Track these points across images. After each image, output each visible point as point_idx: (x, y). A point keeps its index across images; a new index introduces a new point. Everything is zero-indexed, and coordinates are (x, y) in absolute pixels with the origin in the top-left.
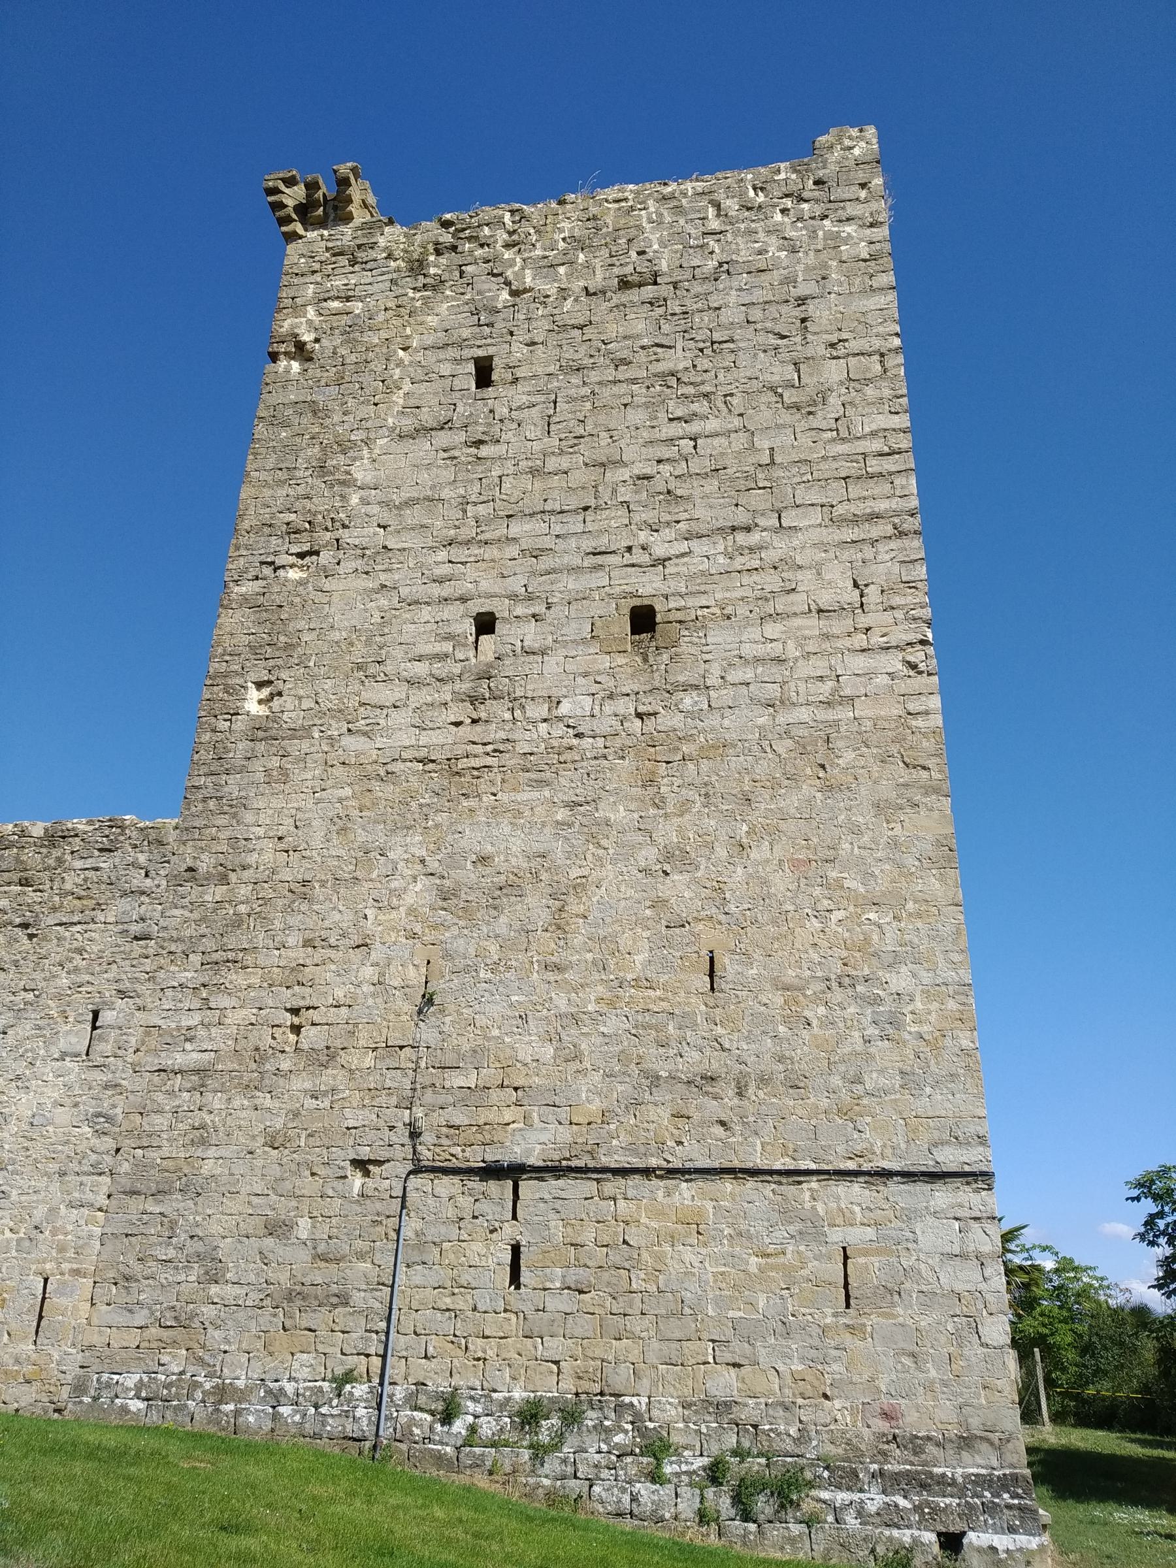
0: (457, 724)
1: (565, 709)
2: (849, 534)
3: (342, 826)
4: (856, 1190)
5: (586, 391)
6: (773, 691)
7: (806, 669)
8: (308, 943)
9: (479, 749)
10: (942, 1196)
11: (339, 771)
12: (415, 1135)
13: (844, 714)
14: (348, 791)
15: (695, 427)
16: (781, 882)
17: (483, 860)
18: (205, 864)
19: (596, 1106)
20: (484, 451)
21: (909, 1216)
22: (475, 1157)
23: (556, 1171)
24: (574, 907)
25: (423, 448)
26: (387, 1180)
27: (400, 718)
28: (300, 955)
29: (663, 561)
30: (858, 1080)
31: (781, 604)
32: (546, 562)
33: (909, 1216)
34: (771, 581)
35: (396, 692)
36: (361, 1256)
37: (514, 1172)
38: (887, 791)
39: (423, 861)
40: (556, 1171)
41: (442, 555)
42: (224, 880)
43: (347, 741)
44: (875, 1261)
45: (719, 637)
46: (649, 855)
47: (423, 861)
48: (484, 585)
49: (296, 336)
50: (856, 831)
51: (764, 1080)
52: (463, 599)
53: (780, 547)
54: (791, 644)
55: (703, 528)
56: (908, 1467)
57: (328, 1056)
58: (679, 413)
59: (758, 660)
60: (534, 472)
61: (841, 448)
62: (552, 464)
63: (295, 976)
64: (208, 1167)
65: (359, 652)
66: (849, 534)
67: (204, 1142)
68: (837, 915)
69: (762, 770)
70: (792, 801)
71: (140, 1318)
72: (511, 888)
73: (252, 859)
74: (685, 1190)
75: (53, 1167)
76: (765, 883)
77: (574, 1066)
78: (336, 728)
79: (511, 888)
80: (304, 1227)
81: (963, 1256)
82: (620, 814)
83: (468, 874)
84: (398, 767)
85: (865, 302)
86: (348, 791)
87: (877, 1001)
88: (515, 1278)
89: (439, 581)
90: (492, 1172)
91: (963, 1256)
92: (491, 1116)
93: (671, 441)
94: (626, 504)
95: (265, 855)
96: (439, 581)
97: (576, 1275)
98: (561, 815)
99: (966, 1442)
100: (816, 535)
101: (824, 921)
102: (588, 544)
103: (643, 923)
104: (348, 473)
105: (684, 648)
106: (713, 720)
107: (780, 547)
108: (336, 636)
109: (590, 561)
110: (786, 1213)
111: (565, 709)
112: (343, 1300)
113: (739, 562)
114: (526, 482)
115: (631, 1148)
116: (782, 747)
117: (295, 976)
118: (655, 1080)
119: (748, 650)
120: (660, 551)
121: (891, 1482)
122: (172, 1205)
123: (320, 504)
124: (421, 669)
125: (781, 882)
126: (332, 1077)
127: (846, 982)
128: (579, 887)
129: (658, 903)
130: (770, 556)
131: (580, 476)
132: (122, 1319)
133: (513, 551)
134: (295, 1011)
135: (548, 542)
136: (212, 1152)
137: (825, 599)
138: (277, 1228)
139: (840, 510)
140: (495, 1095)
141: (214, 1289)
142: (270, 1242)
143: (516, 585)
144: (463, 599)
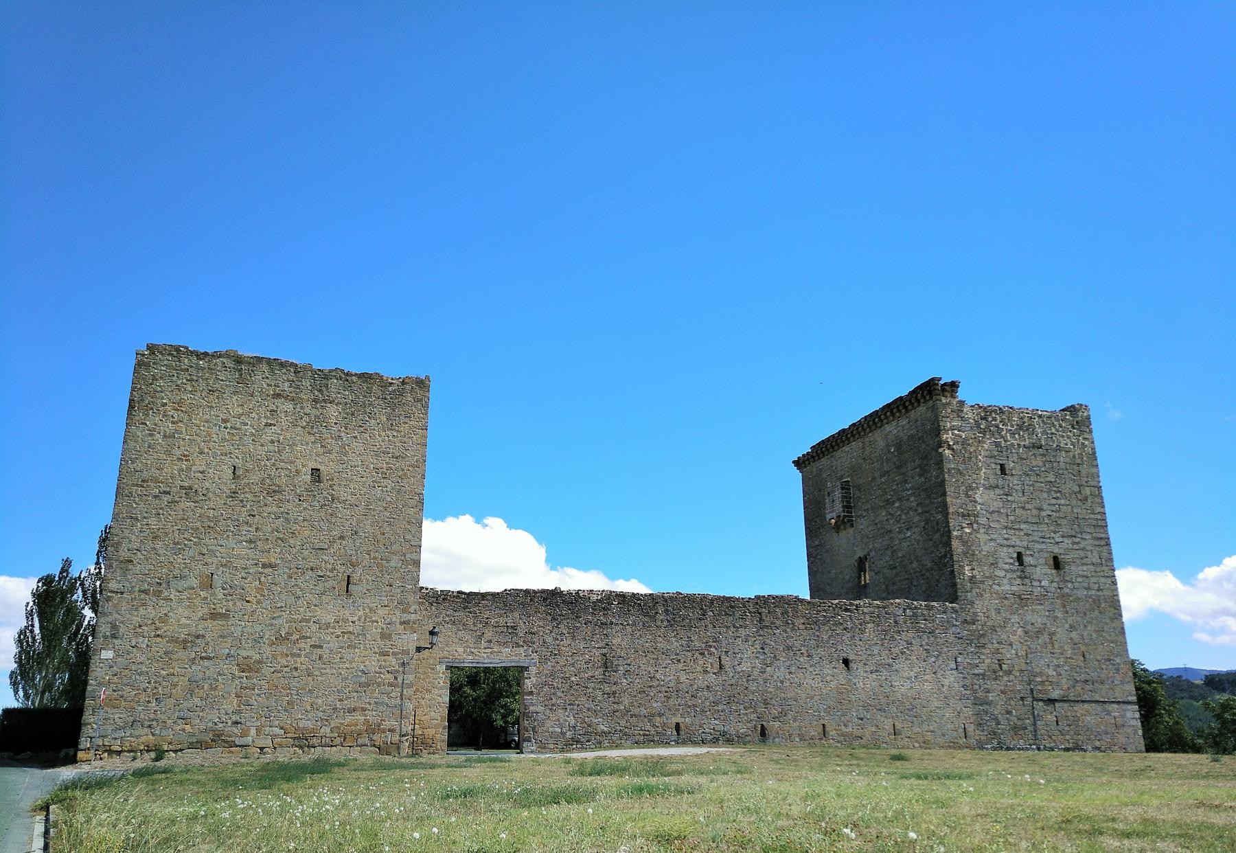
0: (1019, 585)
2: (1096, 543)
4: (1115, 706)
5: (1031, 483)
8: (998, 643)
9: (1025, 593)
11: (994, 595)
13: (1100, 593)
14: (997, 601)
15: (1059, 502)
19: (1066, 686)
21: (1124, 710)
24: (1054, 638)
25: (991, 493)
27: (1005, 581)
29: (1057, 543)
30: (1113, 682)
31: (1085, 561)
32: (1031, 538)
33: (1124, 710)
34: (1082, 554)
36: (1027, 719)
38: (1111, 614)
39: (1019, 623)
43: (994, 586)
44: (1120, 719)
46: (1067, 626)
47: (1019, 623)
48: (1017, 543)
49: (948, 442)
50: (1107, 624)
52: (1013, 546)
54: (1089, 573)
55: (1066, 535)
56: (35, 616)
57: (1009, 673)
58: (1054, 496)
59: (1083, 576)
61: (1092, 516)
63: (997, 651)
64: (991, 698)
65: (991, 560)
66: (1096, 543)
67: (988, 692)
68: (1106, 644)
70: (1093, 615)
71: (986, 733)
73: (979, 618)
74: (1086, 706)
75: (958, 698)
76: (1091, 636)
77: (1060, 677)
81: (1134, 718)
82: (1059, 615)
83: (1029, 627)
84: (1007, 596)
85: (36, 615)
86: (997, 601)
87: (1114, 665)
88: (1058, 725)
89: (1006, 539)
91: (1134, 718)
92: (1046, 688)
94: (1047, 524)
96: (1006, 539)
97: (1069, 722)
98: (1047, 613)
100: (1091, 541)
101: (1103, 645)
103: (1068, 643)
104: (974, 498)
106: (1075, 592)
108: (983, 553)
110: (1104, 710)
111: (1043, 584)
115: (1074, 696)
116: (1090, 600)
117: (997, 651)
118: (1077, 681)
119: (1080, 573)
120: (1057, 540)
126: (1012, 677)
127: (1109, 660)
128: (1054, 633)
129: (1071, 639)
130: (1081, 546)
132: (982, 733)
134: (999, 660)
135: (1030, 532)
136: (990, 695)
139: (1094, 535)
140: (1046, 683)
141: (999, 726)
142: (1008, 716)
144: (1013, 546)
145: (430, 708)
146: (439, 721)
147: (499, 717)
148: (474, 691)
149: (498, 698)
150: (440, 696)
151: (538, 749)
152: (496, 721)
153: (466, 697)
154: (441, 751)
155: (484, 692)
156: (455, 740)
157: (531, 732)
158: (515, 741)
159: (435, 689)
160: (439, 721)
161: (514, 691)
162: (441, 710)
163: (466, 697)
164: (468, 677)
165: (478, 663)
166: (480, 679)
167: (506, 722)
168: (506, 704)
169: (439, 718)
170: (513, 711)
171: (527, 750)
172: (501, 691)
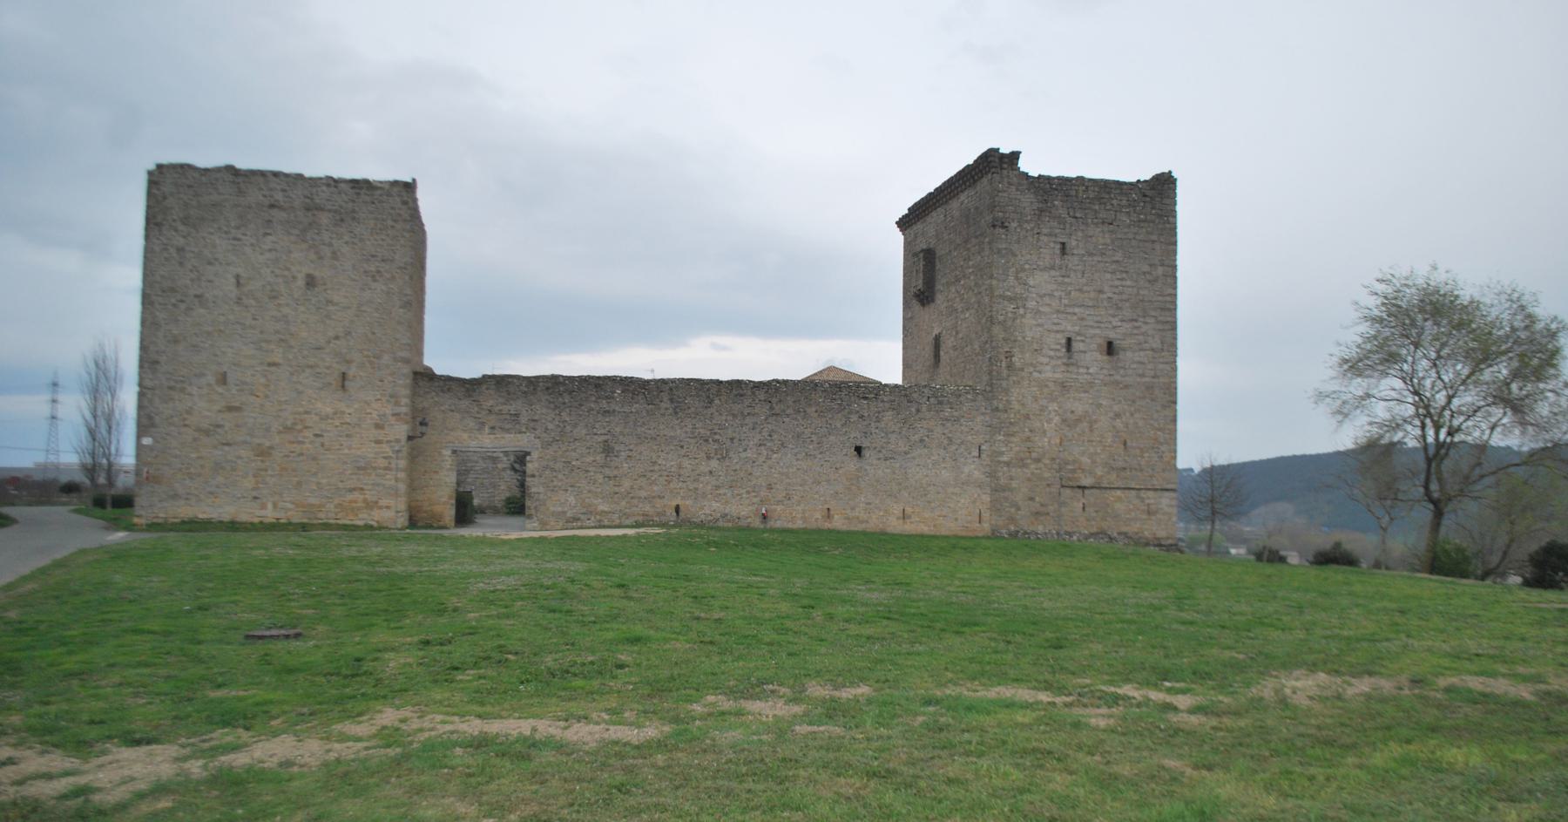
1: (1091, 371)
3: (1036, 399)
6: (1141, 372)
7: (1150, 367)
10: (1167, 494)
12: (1061, 479)
16: (1141, 423)
17: (1072, 412)
18: (1001, 406)
20: (1071, 369)
22: (1075, 484)
23: (1092, 487)
26: (1054, 489)
27: (1048, 368)
28: (1028, 434)
32: (1085, 323)
35: (1045, 360)
37: (1084, 488)
40: (1092, 487)
41: (1055, 316)
42: (1006, 411)
45: (1129, 354)
46: (1112, 415)
51: (1136, 469)
53: (1144, 328)
57: (1038, 460)
60: (1080, 290)
61: (1160, 298)
62: (1085, 288)
67: (1011, 479)
69: (1138, 394)
72: (1079, 421)
78: (1031, 369)
79: (1079, 421)
80: (1037, 499)
90: (1079, 487)
93: (1117, 287)
95: (1016, 406)
99: (1168, 538)
102: (1096, 319)
105: (1121, 356)
106: (1127, 378)
107: (1144, 328)
109: (1096, 325)
111: (1091, 371)
112: (1048, 514)
113: (1135, 331)
114: (1078, 294)
117: (1028, 439)
118: (1113, 469)
120: (1114, 324)
121: (955, 249)
122: (1007, 494)
123: (1018, 290)
124: (1052, 353)
125: (1141, 423)
128: (1096, 421)
129: (1114, 427)
130: (1143, 330)
131: (1092, 295)
133: (1075, 318)
137: (1154, 346)
138: (1032, 499)
143: (1077, 328)
144: (1063, 331)
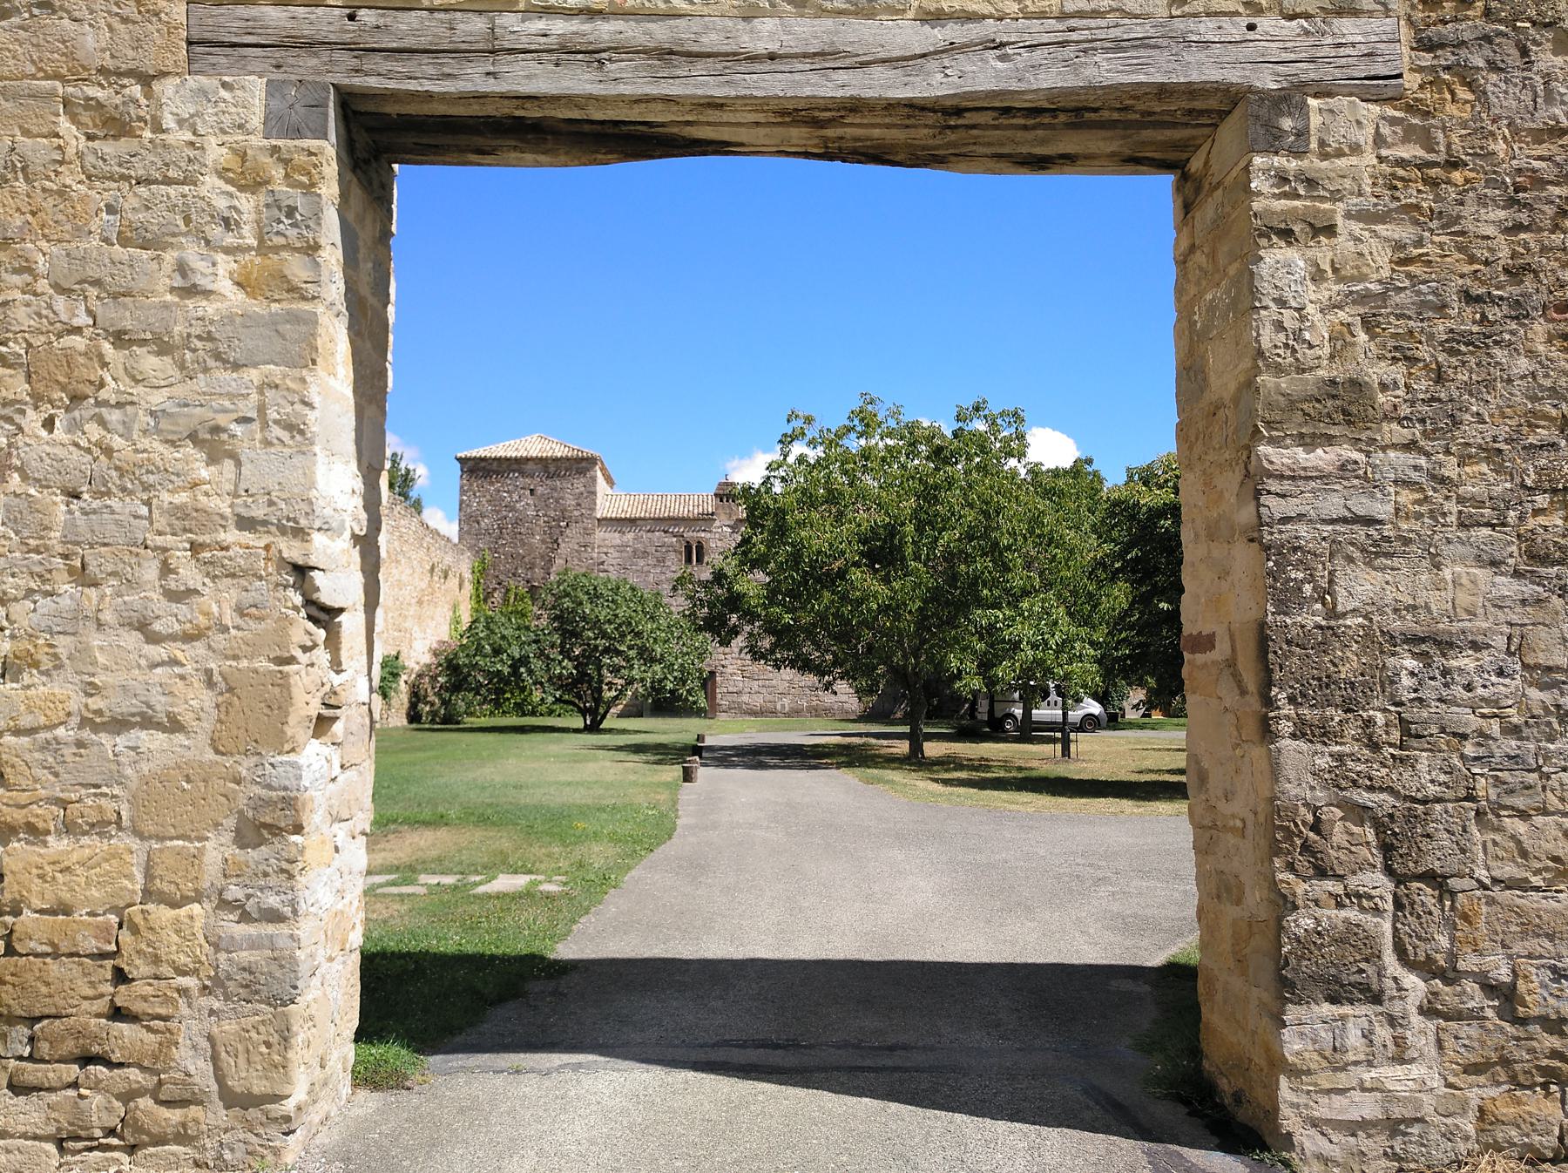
145: (82, 576)
146: (194, 747)
147: (971, 666)
148: (886, 580)
149: (962, 607)
150: (213, 444)
151: (1479, 1092)
152: (959, 676)
153: (859, 602)
154: (216, 1115)
155: (917, 585)
156: (886, 705)
157: (1377, 882)
158: (1012, 716)
159: (150, 363)
160: (194, 747)
161: (1018, 583)
162: (219, 601)
163: (859, 602)
164: (864, 541)
165: (665, 54)
166: (902, 543)
167: (991, 682)
168: (991, 626)
169: (197, 701)
170: (1016, 646)
171: (1326, 1108)
172: (974, 582)
